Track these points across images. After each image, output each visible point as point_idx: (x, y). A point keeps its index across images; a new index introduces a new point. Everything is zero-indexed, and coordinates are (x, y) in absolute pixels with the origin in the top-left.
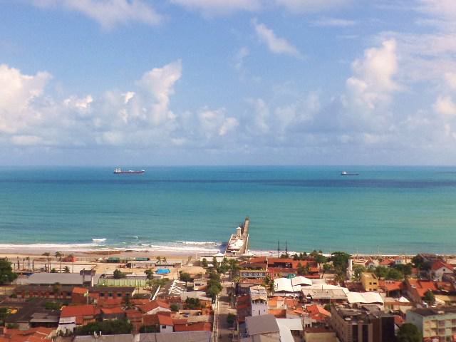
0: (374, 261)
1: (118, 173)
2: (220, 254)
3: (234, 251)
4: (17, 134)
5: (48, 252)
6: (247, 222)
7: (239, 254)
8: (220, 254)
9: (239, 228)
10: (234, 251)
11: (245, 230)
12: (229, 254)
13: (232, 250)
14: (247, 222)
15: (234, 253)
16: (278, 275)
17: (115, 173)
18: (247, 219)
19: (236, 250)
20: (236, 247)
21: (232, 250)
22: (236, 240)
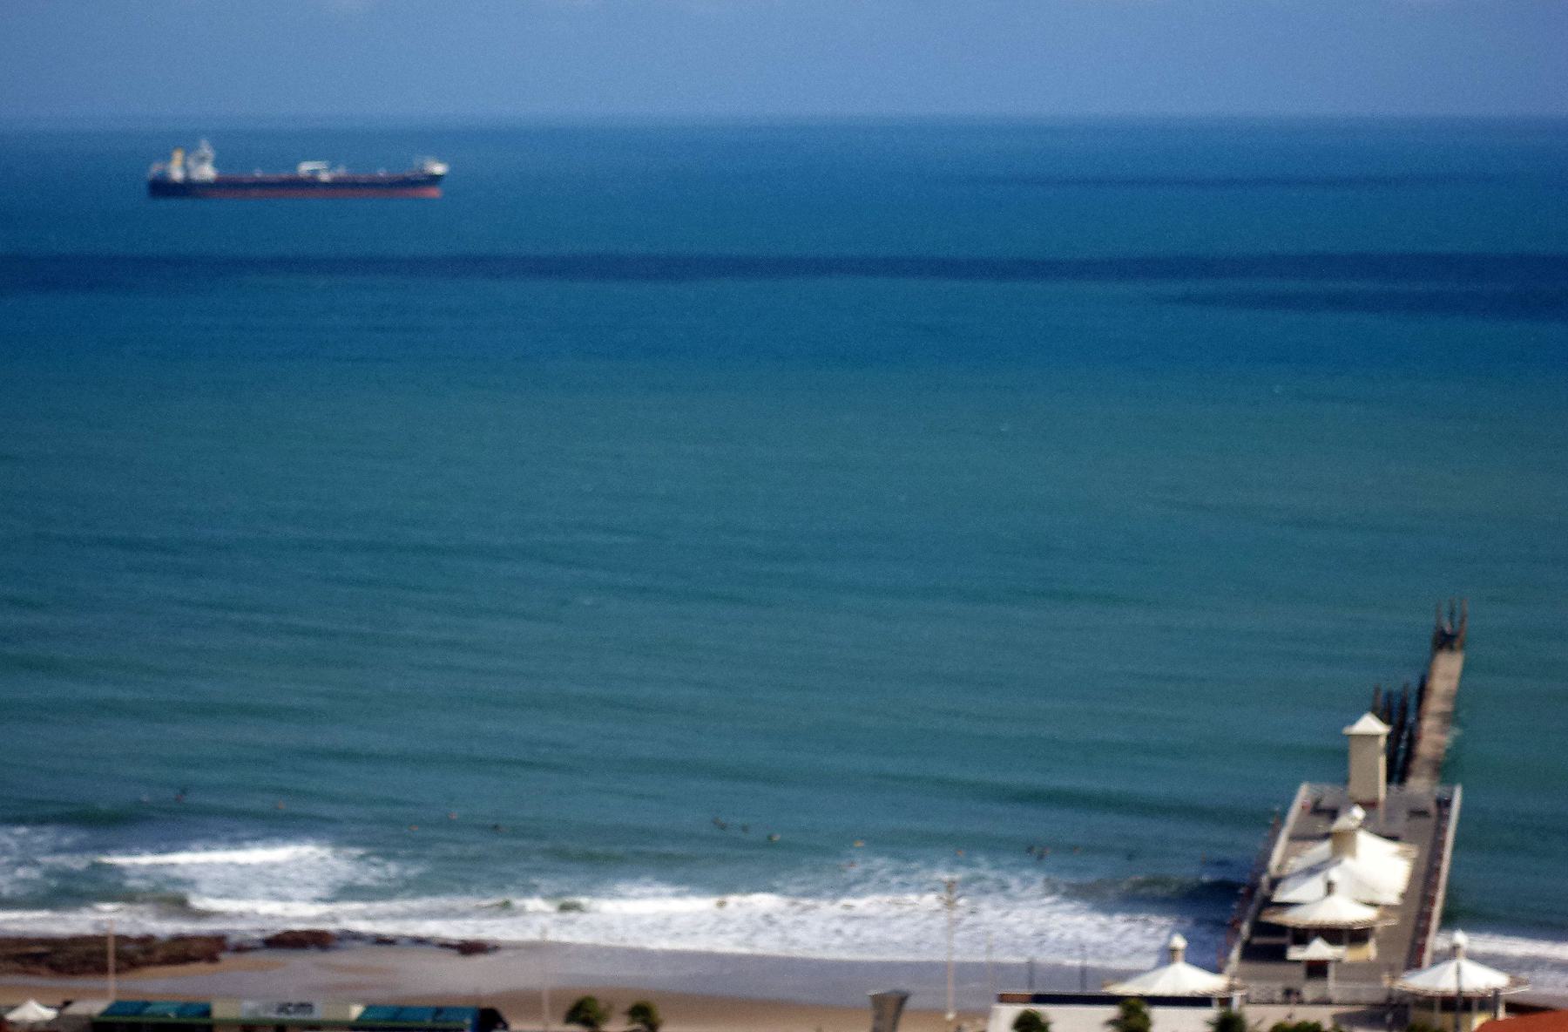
0: (1016, 920)
1: (188, 189)
2: (1189, 979)
3: (1318, 950)
4: (550, 913)
5: (1396, 835)
6: (1447, 671)
7: (1368, 971)
8: (1189, 979)
9: (1370, 725)
10: (1318, 950)
11: (1432, 738)
12: (1272, 979)
13: (1303, 936)
14: (1447, 671)
15: (1317, 969)
16: (478, 890)
17: (162, 188)
18: (1444, 641)
19: (1333, 934)
20: (1344, 910)
21: (1303, 936)
22: (1342, 843)
